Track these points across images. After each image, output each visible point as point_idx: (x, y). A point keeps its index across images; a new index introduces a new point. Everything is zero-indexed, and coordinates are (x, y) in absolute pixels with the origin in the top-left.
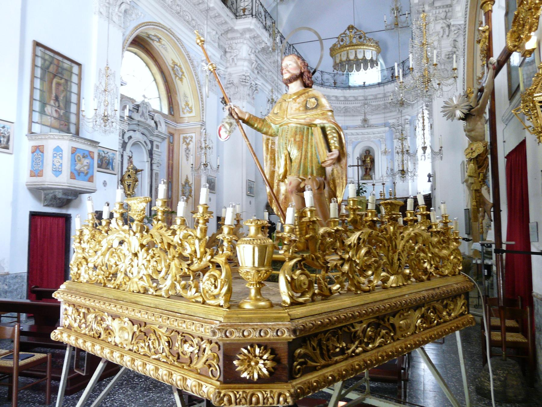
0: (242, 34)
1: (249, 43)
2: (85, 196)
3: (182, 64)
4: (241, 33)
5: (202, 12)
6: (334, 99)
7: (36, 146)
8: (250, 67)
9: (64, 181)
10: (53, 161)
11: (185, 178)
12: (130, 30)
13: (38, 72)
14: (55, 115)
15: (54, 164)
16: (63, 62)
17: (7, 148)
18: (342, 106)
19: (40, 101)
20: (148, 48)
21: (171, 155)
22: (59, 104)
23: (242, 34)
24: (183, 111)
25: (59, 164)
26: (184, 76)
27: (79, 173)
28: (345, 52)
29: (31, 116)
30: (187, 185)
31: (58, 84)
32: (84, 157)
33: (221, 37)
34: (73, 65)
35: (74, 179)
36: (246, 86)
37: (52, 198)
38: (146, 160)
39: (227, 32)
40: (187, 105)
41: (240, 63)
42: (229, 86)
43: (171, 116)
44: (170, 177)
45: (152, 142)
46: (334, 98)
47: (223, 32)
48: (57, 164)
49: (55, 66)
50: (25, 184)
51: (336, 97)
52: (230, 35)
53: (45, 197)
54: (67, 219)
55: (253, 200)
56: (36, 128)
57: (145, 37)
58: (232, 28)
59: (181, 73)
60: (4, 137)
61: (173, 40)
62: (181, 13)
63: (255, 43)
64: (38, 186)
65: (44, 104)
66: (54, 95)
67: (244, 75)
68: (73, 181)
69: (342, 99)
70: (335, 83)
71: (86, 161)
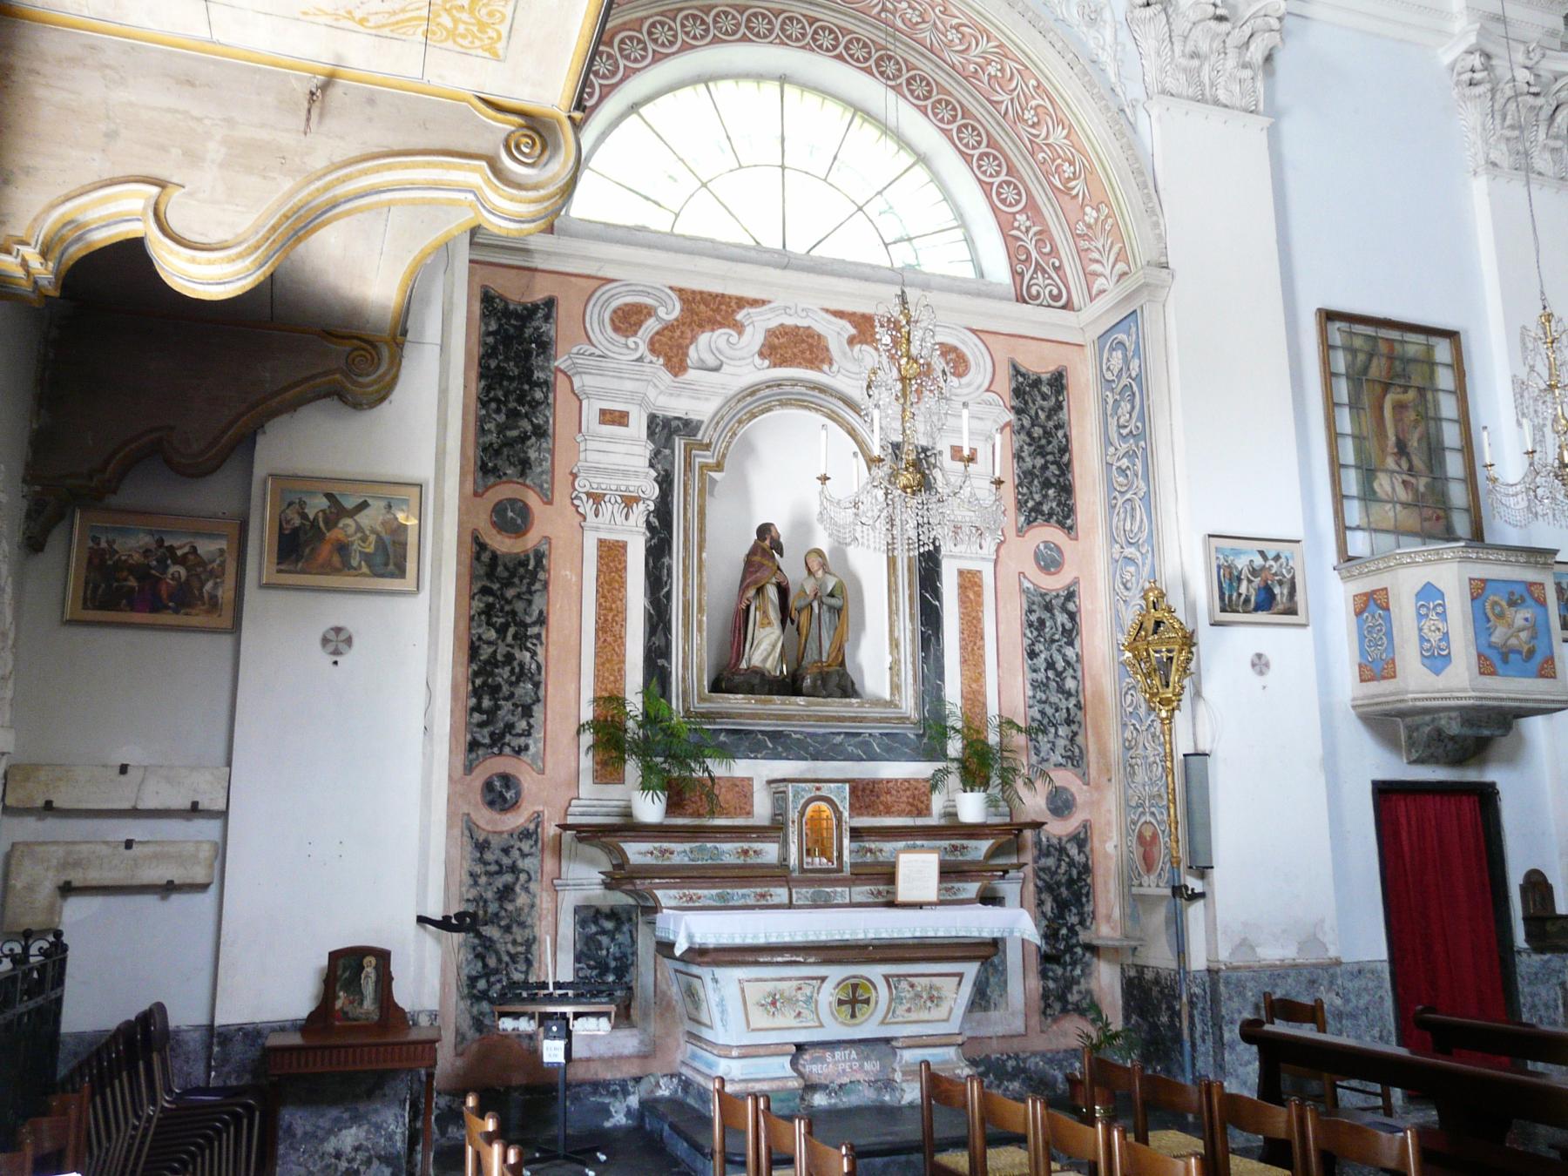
7: (1365, 594)
9: (1461, 682)
10: (1420, 630)
13: (1342, 390)
14: (1402, 494)
15: (1422, 639)
16: (1403, 342)
19: (1357, 467)
25: (1438, 635)
27: (1505, 654)
31: (1400, 407)
32: (1512, 603)
34: (1433, 340)
35: (1493, 673)
48: (1435, 637)
49: (1383, 361)
53: (1410, 737)
54: (1486, 796)
56: (1359, 543)
60: (1281, 583)
65: (1368, 473)
66: (1392, 439)
71: (1520, 616)
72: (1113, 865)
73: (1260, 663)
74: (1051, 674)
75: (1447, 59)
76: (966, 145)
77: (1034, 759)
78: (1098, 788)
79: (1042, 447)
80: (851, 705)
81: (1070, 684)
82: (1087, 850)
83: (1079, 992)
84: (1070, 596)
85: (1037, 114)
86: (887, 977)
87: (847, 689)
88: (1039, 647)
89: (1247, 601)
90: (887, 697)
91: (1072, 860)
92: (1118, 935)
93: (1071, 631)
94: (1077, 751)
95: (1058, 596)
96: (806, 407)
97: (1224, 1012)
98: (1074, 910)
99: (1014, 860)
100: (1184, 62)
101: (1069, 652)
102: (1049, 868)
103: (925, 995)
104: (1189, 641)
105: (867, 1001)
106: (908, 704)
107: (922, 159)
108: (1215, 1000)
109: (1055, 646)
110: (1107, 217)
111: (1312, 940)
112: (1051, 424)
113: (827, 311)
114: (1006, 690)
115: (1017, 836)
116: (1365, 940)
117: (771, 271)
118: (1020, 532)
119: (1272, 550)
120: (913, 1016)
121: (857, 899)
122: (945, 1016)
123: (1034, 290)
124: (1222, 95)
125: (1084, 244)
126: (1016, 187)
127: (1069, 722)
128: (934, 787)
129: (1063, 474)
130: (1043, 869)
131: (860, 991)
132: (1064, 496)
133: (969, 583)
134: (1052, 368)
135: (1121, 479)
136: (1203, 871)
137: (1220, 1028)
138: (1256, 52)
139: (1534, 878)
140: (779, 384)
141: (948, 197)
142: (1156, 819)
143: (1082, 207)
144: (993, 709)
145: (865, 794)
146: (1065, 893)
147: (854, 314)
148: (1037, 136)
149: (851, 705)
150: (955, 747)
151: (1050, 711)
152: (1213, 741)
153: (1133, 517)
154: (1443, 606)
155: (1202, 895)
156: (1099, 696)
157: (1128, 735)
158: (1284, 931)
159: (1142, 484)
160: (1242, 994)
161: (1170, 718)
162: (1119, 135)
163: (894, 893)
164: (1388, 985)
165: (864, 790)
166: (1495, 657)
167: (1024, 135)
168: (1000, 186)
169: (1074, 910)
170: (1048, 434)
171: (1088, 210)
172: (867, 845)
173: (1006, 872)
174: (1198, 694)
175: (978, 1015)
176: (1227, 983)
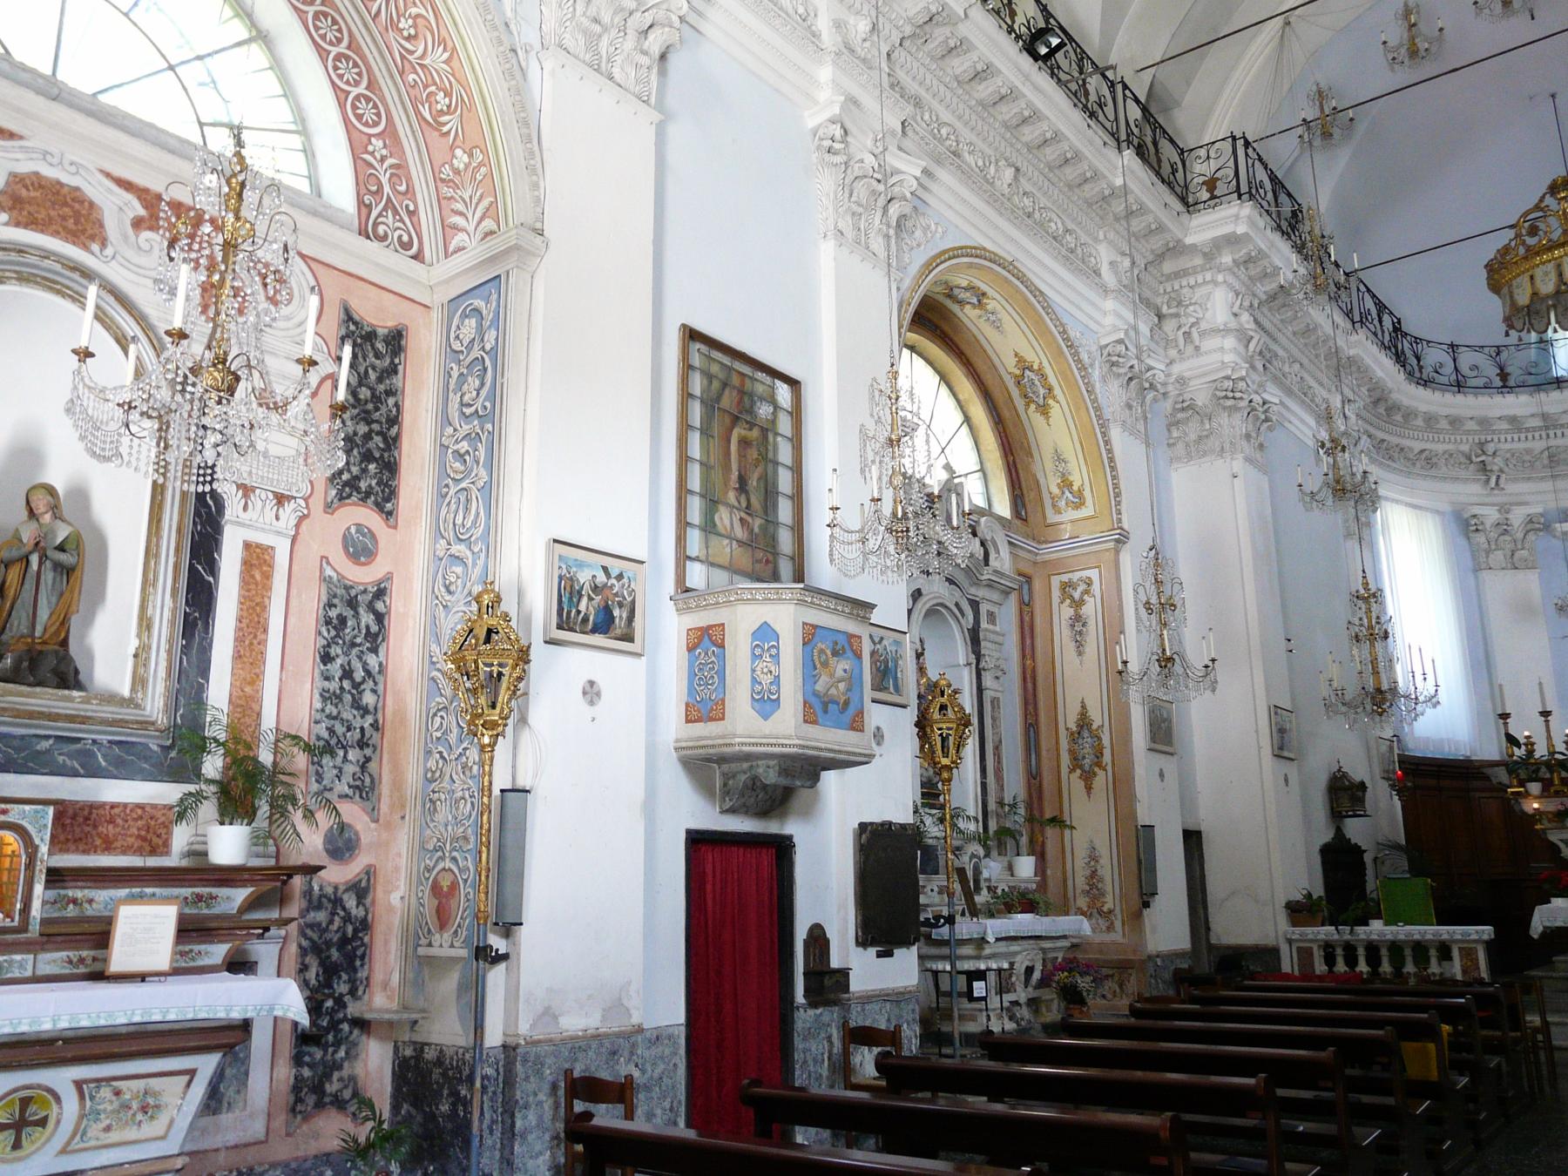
0: (1209, 257)
1: (1231, 279)
2: (830, 778)
3: (1045, 364)
4: (1205, 254)
5: (1090, 205)
6: (1506, 426)
7: (700, 629)
8: (1242, 349)
9: (785, 729)
10: (753, 671)
11: (1079, 709)
12: (910, 283)
13: (696, 413)
14: (739, 532)
15: (754, 681)
16: (753, 379)
17: (628, 638)
18: (1539, 445)
19: (702, 496)
20: (946, 328)
21: (1028, 642)
22: (748, 500)
23: (1209, 257)
24: (1054, 506)
25: (770, 678)
26: (1054, 398)
27: (826, 703)
28: (1550, 267)
29: (681, 540)
30: (1086, 734)
31: (744, 443)
32: (835, 653)
33: (1145, 277)
34: (778, 383)
35: (815, 722)
36: (1237, 409)
37: (745, 785)
38: (962, 661)
39: (1161, 257)
40: (1066, 484)
41: (1209, 344)
42: (1180, 416)
43: (1018, 522)
44: (1031, 708)
45: (975, 605)
46: (1505, 426)
47: (1151, 258)
48: (766, 680)
49: (735, 393)
50: (672, 746)
51: (1513, 420)
52: (1168, 267)
53: (725, 785)
54: (782, 849)
55: (1292, 770)
56: (697, 575)
57: (941, 298)
58: (1179, 241)
59: (1042, 391)
60: (621, 605)
61: (1022, 293)
62: (1037, 215)
63: (1250, 278)
64: (712, 751)
65: (712, 503)
66: (735, 475)
67: (1228, 378)
68: (810, 729)
69: (1537, 422)
70: (1504, 376)
71: (841, 666)
72: (396, 921)
73: (591, 692)
74: (346, 684)
75: (811, 123)
76: (323, 37)
77: (315, 787)
78: (389, 826)
79: (367, 412)
80: (71, 699)
81: (368, 699)
82: (368, 901)
83: (341, 1079)
84: (380, 593)
85: (415, 26)
86: (79, 1085)
87: (67, 676)
88: (335, 650)
89: (585, 620)
90: (126, 693)
91: (348, 913)
92: (394, 1006)
93: (377, 635)
94: (368, 780)
95: (365, 591)
96: (58, 292)
97: (518, 1095)
98: (345, 977)
99: (275, 915)
100: (586, 22)
101: (372, 660)
102: (319, 924)
103: (135, 1105)
104: (523, 656)
105: (43, 1122)
106: (155, 705)
107: (261, 36)
108: (509, 1081)
109: (355, 651)
110: (481, 164)
111: (617, 1006)
112: (381, 387)
113: (108, 175)
114: (288, 697)
115: (284, 883)
116: (667, 1008)
117: (31, 95)
118: (329, 508)
119: (616, 566)
120: (114, 1136)
121: (45, 969)
122: (161, 1133)
123: (381, 229)
124: (616, 72)
125: (446, 191)
126: (375, 106)
127: (362, 744)
128: (181, 816)
129: (388, 448)
130: (311, 926)
131: (32, 1108)
132: (386, 474)
133: (257, 559)
134: (390, 324)
135: (457, 465)
136: (508, 928)
137: (513, 1116)
138: (655, 42)
139: (816, 932)
140: (21, 250)
141: (289, 92)
142: (464, 867)
143: (452, 149)
144: (268, 721)
145: (75, 823)
146: (335, 958)
147: (146, 191)
148: (412, 53)
149: (71, 699)
150: (213, 765)
151: (340, 729)
152: (535, 776)
153: (467, 509)
154: (777, 648)
155: (505, 957)
156: (402, 720)
157: (431, 764)
158: (590, 997)
159: (483, 473)
160: (539, 1073)
161: (493, 745)
162: (509, 74)
163: (105, 961)
164: (682, 1051)
165: (74, 817)
166: (818, 708)
167: (395, 46)
168: (357, 98)
169: (345, 977)
170: (376, 399)
171: (458, 152)
172: (70, 893)
173: (267, 929)
174: (523, 720)
175: (207, 1121)
176: (525, 1061)
